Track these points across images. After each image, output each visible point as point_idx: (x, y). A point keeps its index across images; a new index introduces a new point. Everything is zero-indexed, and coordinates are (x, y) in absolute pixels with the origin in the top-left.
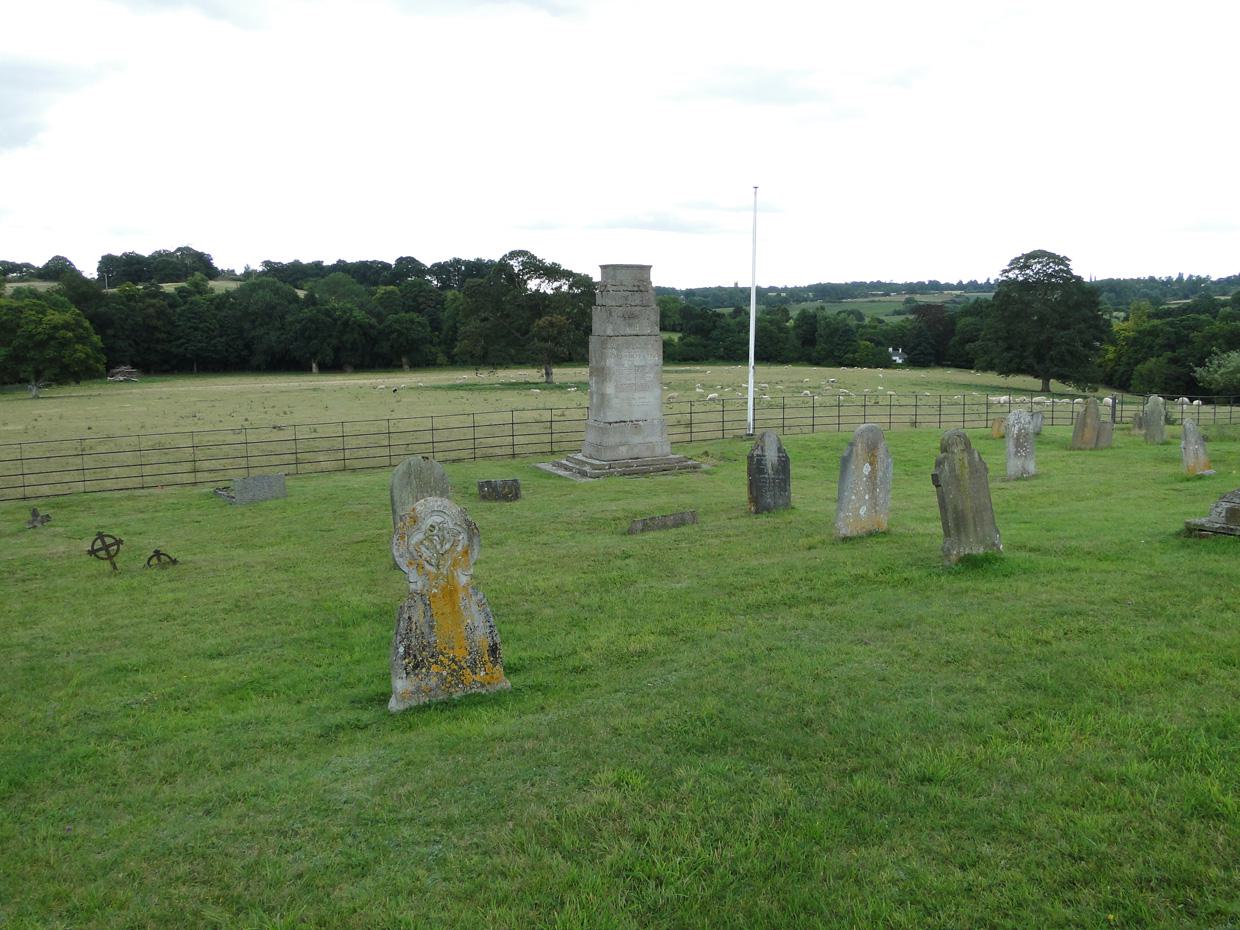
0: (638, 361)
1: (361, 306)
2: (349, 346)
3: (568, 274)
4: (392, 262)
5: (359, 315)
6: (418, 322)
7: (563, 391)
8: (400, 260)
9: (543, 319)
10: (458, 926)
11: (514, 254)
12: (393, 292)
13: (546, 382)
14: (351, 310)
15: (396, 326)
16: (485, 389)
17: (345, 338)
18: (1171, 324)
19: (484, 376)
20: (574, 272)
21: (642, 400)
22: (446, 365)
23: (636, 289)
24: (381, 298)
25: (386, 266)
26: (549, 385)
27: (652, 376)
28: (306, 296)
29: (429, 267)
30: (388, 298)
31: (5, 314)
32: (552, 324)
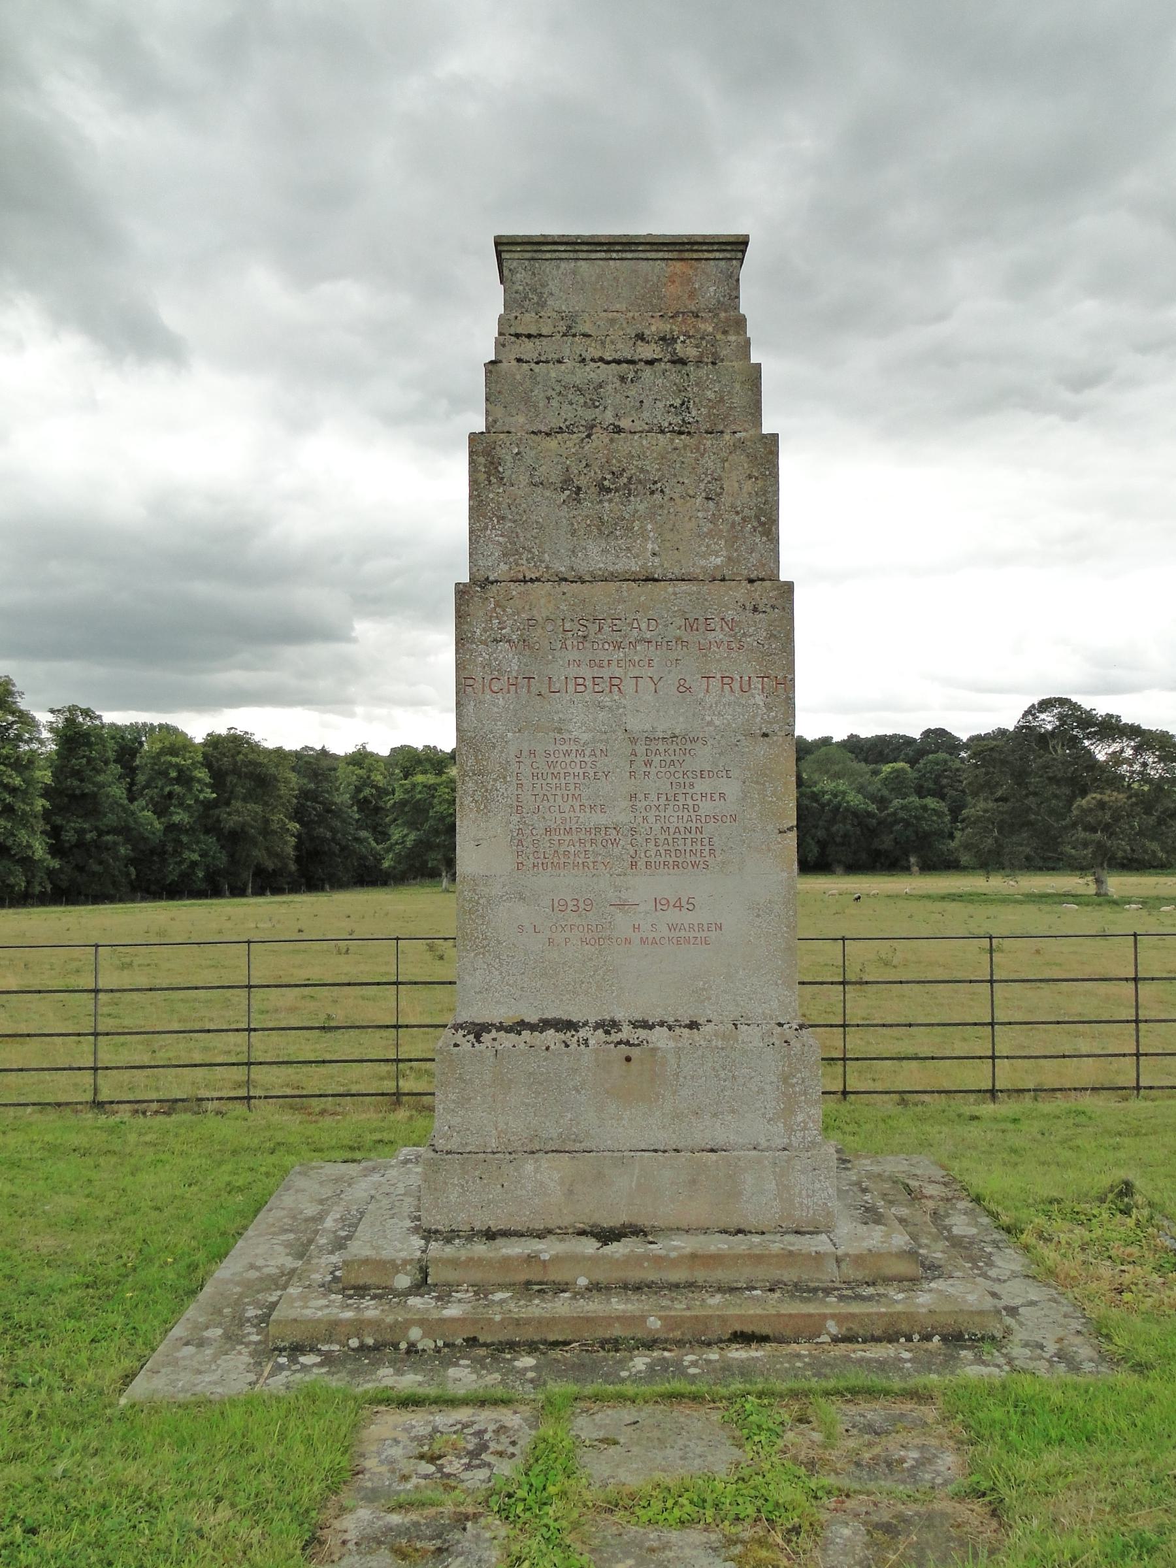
1: (860, 789)
2: (838, 840)
3: (1134, 731)
5: (855, 800)
6: (934, 809)
7: (1117, 909)
8: (927, 733)
9: (1088, 798)
11: (1045, 705)
12: (903, 769)
13: (1097, 895)
14: (844, 793)
15: (902, 814)
16: (992, 901)
17: (834, 829)
19: (996, 883)
20: (1144, 727)
21: (673, 916)
22: (973, 868)
23: (647, 351)
24: (886, 779)
25: (909, 741)
26: (1102, 899)
27: (732, 789)
29: (965, 741)
30: (897, 777)
31: (420, 792)
32: (1102, 805)
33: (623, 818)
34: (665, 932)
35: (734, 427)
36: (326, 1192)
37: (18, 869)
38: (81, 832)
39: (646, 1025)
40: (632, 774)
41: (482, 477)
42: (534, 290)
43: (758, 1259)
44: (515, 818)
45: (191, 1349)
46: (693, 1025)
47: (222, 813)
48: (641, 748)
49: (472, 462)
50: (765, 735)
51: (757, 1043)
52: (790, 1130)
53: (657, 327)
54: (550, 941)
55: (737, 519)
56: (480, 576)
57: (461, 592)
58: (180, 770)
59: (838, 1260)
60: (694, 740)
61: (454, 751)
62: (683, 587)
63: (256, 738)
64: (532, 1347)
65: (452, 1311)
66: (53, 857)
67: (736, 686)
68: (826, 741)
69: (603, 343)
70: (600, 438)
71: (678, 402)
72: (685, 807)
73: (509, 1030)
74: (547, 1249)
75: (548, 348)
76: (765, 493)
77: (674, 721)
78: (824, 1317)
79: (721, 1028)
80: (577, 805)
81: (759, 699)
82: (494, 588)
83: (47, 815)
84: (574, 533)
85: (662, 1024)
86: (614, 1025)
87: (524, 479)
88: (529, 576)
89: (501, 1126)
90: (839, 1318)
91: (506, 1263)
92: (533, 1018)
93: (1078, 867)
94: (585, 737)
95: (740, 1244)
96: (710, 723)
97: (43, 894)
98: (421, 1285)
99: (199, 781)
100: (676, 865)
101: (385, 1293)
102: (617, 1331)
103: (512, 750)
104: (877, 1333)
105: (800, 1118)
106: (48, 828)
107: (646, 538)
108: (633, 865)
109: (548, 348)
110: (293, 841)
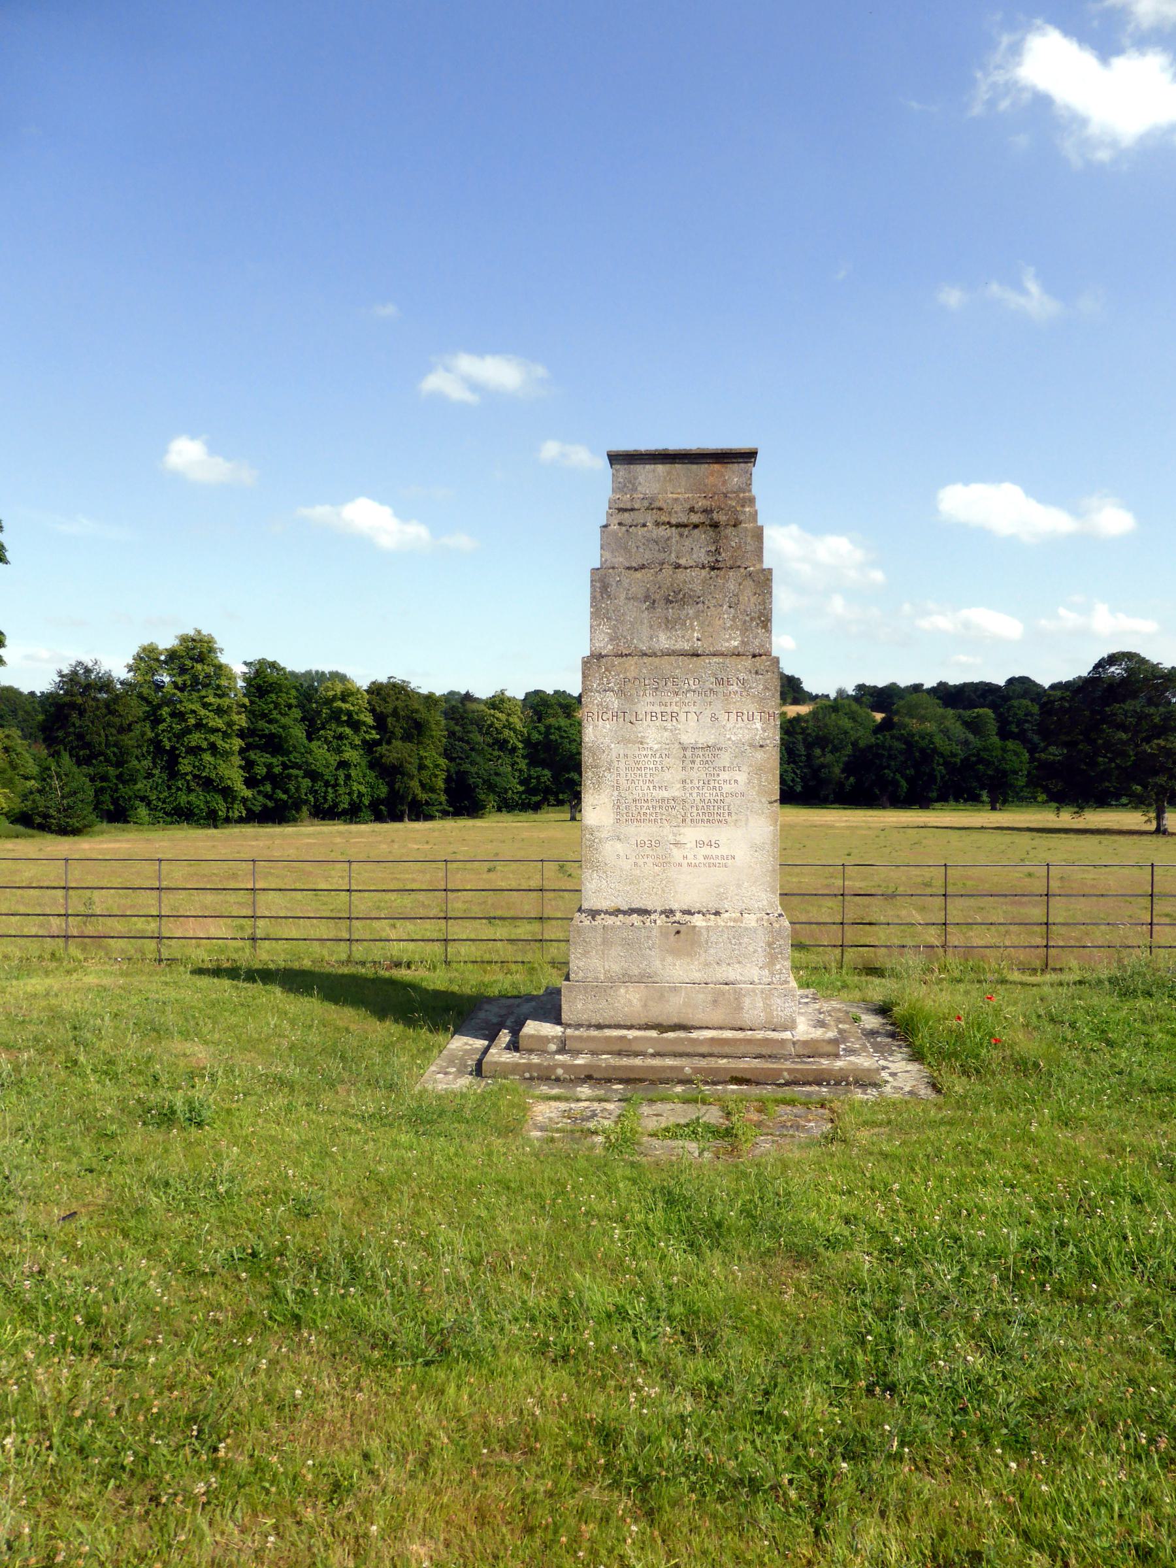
0: (692, 731)
4: (1002, 683)
8: (1011, 681)
10: (1173, 1453)
11: (1112, 659)
12: (986, 715)
14: (931, 736)
18: (567, 1114)
19: (1066, 818)
21: (706, 851)
23: (695, 518)
27: (742, 777)
28: (883, 719)
33: (677, 794)
34: (702, 860)
35: (748, 564)
36: (503, 1012)
37: (219, 798)
38: (269, 766)
39: (689, 912)
40: (684, 768)
41: (598, 595)
42: (630, 482)
43: (749, 1041)
44: (616, 793)
45: (441, 1076)
46: (717, 913)
47: (382, 749)
48: (689, 753)
49: (592, 586)
50: (761, 746)
51: (754, 924)
52: (772, 974)
53: (701, 504)
54: (636, 864)
55: (747, 618)
56: (597, 652)
57: (586, 663)
58: (349, 714)
59: (794, 1043)
60: (719, 749)
61: (580, 696)
62: (715, 659)
63: (412, 686)
64: (621, 1081)
65: (580, 1061)
66: (248, 788)
67: (745, 717)
68: (917, 688)
69: (670, 513)
70: (668, 571)
71: (713, 549)
72: (714, 788)
73: (611, 914)
74: (631, 1034)
75: (639, 517)
76: (764, 603)
77: (708, 737)
78: (781, 1070)
79: (734, 915)
80: (651, 786)
81: (758, 725)
82: (604, 660)
83: (242, 751)
84: (651, 627)
85: (699, 912)
86: (672, 912)
87: (623, 596)
88: (625, 652)
89: (607, 967)
90: (789, 1071)
91: (608, 1039)
92: (625, 908)
93: (1138, 802)
94: (656, 747)
95: (739, 1035)
96: (729, 739)
97: (241, 817)
98: (562, 1050)
99: (364, 723)
100: (708, 821)
101: (543, 1052)
102: (668, 1075)
103: (614, 754)
104: (811, 1079)
105: (778, 967)
106: (243, 763)
107: (694, 630)
108: (684, 821)
109: (639, 517)
110: (443, 775)
